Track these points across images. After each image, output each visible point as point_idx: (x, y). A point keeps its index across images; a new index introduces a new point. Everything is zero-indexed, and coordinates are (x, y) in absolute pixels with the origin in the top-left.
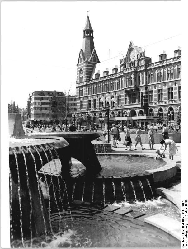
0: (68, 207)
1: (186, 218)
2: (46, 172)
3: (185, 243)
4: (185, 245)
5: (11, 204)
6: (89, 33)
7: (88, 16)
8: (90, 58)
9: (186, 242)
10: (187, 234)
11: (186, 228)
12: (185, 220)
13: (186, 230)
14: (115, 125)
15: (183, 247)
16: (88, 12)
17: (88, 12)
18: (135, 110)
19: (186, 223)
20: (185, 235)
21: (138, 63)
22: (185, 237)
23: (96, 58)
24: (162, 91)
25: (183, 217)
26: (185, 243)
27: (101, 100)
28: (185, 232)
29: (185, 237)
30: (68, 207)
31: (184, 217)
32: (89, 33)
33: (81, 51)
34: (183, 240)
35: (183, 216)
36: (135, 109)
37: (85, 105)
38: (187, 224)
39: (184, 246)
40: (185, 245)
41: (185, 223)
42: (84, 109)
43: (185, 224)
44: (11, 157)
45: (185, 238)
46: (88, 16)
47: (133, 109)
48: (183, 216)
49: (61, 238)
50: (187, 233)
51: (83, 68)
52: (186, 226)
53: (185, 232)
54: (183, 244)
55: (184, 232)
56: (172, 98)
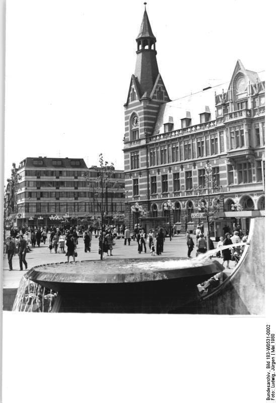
3: (271, 393)
4: (271, 396)
6: (147, 41)
7: (145, 12)
8: (149, 88)
9: (273, 392)
10: (274, 379)
11: (273, 369)
12: (272, 356)
13: (272, 372)
16: (145, 4)
17: (145, 4)
19: (273, 361)
20: (271, 380)
21: (254, 103)
22: (271, 383)
26: (271, 393)
28: (271, 375)
29: (271, 383)
32: (147, 41)
33: (134, 79)
34: (269, 389)
38: (275, 363)
39: (270, 398)
40: (271, 396)
43: (271, 362)
45: (271, 385)
46: (145, 12)
50: (275, 378)
52: (273, 366)
53: (271, 376)
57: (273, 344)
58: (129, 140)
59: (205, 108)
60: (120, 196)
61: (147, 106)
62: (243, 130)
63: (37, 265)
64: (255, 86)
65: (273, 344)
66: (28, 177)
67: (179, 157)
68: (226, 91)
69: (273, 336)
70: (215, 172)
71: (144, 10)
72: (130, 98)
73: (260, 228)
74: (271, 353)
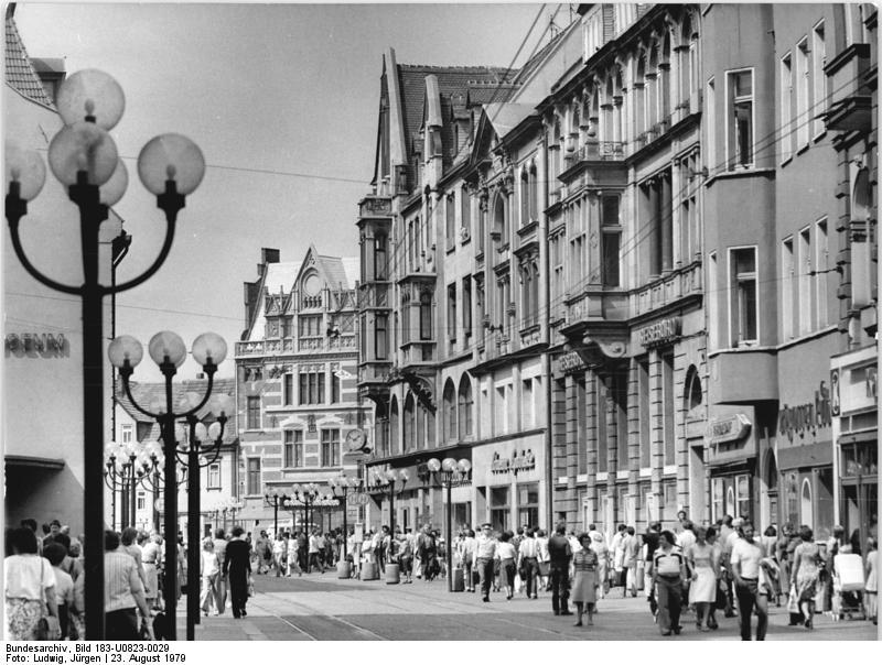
0: (139, 627)
1: (110, 658)
2: (707, 517)
3: (21, 654)
4: (16, 654)
5: (162, 495)
10: (52, 660)
11: (75, 659)
12: (102, 655)
13: (67, 657)
14: (507, 531)
15: (9, 647)
19: (92, 658)
20: (51, 654)
22: (44, 654)
24: (338, 437)
25: (113, 646)
26: (21, 654)
27: (692, 517)
28: (61, 653)
29: (44, 654)
30: (139, 627)
31: (114, 652)
34: (31, 649)
35: (119, 648)
39: (11, 652)
40: (16, 654)
41: (94, 653)
43: (90, 654)
44: (159, 334)
45: (39, 654)
48: (119, 648)
49: (131, 353)
50: (55, 663)
52: (81, 659)
53: (60, 654)
54: (17, 649)
55: (59, 650)
58: (608, 311)
60: (426, 300)
61: (483, 589)
62: (323, 374)
64: (336, 295)
66: (178, 634)
68: (287, 291)
70: (328, 438)
72: (453, 520)
74: (109, 654)
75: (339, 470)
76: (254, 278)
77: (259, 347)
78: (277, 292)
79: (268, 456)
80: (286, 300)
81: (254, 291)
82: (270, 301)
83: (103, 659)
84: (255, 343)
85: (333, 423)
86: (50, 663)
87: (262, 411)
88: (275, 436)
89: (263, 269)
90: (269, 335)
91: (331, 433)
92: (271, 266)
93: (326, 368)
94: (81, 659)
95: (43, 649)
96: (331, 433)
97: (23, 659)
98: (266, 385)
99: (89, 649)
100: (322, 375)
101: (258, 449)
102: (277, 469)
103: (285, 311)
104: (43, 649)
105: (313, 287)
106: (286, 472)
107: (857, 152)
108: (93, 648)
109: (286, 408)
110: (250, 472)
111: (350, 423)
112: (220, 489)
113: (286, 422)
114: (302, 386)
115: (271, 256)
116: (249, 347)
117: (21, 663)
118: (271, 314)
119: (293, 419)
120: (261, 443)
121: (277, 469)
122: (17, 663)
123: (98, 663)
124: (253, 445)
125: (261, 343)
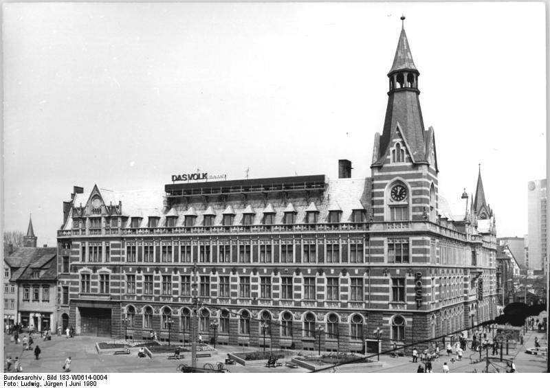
3: (13, 381)
4: (10, 381)
6: (403, 79)
7: (403, 32)
9: (15, 384)
10: (33, 385)
11: (47, 384)
12: (64, 382)
13: (42, 383)
15: (5, 377)
16: (403, 18)
17: (403, 18)
18: (403, 317)
20: (33, 381)
22: (28, 381)
23: (402, 150)
26: (13, 381)
29: (28, 381)
32: (403, 79)
34: (19, 378)
36: (404, 315)
37: (410, 290)
38: (54, 386)
39: (7, 380)
41: (58, 380)
42: (409, 303)
43: (56, 381)
46: (403, 32)
47: (400, 314)
50: (34, 387)
51: (413, 189)
52: (50, 384)
53: (37, 381)
55: (37, 379)
56: (402, 298)
57: (82, 384)
59: (432, 366)
63: (496, 224)
65: (82, 384)
67: (244, 338)
69: (94, 384)
71: (401, 30)
73: (306, 295)
75: (108, 295)
76: (69, 199)
77: (69, 233)
78: (79, 206)
79: (72, 286)
80: (82, 209)
81: (68, 206)
82: (75, 210)
83: (64, 384)
84: (67, 231)
85: (86, 272)
86: (31, 387)
87: (70, 264)
88: (76, 277)
89: (73, 196)
90: (75, 227)
91: (86, 276)
92: (78, 195)
93: (341, 243)
94: (50, 384)
95: (27, 378)
96: (86, 276)
97: (15, 384)
98: (72, 251)
99: (55, 378)
100: (101, 248)
101: (68, 282)
102: (76, 293)
103: (82, 215)
104: (27, 378)
105: (97, 204)
106: (81, 295)
107: (492, 218)
108: (58, 378)
109: (83, 263)
110: (64, 293)
111: (115, 272)
112: (48, 301)
113: (82, 270)
114: (91, 252)
115: (79, 190)
116: (64, 233)
117: (13, 387)
118: (75, 217)
119: (85, 269)
120: (69, 280)
121: (76, 293)
122: (10, 387)
123: (61, 387)
124: (65, 280)
125: (70, 231)
